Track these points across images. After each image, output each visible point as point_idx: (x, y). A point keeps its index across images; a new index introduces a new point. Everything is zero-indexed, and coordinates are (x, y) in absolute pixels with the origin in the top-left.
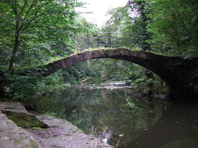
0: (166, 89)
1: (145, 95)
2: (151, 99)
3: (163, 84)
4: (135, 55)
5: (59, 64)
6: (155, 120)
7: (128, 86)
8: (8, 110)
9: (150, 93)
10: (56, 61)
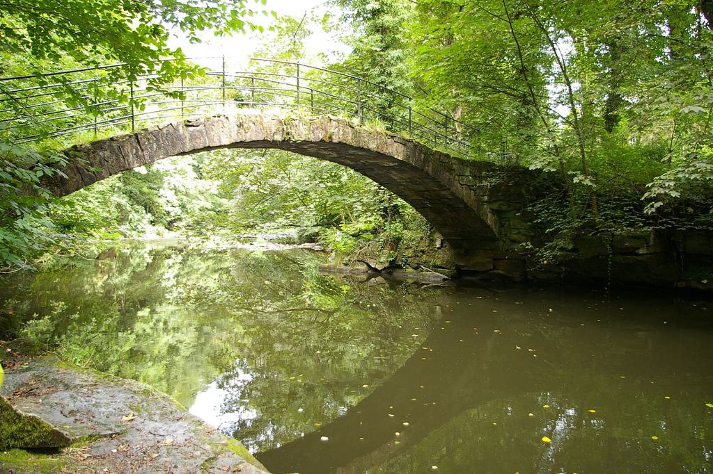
0: (441, 257)
1: (376, 272)
2: (394, 284)
3: (432, 241)
4: (373, 146)
5: (113, 151)
6: (405, 351)
7: (308, 245)
8: (31, 414)
9: (393, 266)
10: (103, 142)
